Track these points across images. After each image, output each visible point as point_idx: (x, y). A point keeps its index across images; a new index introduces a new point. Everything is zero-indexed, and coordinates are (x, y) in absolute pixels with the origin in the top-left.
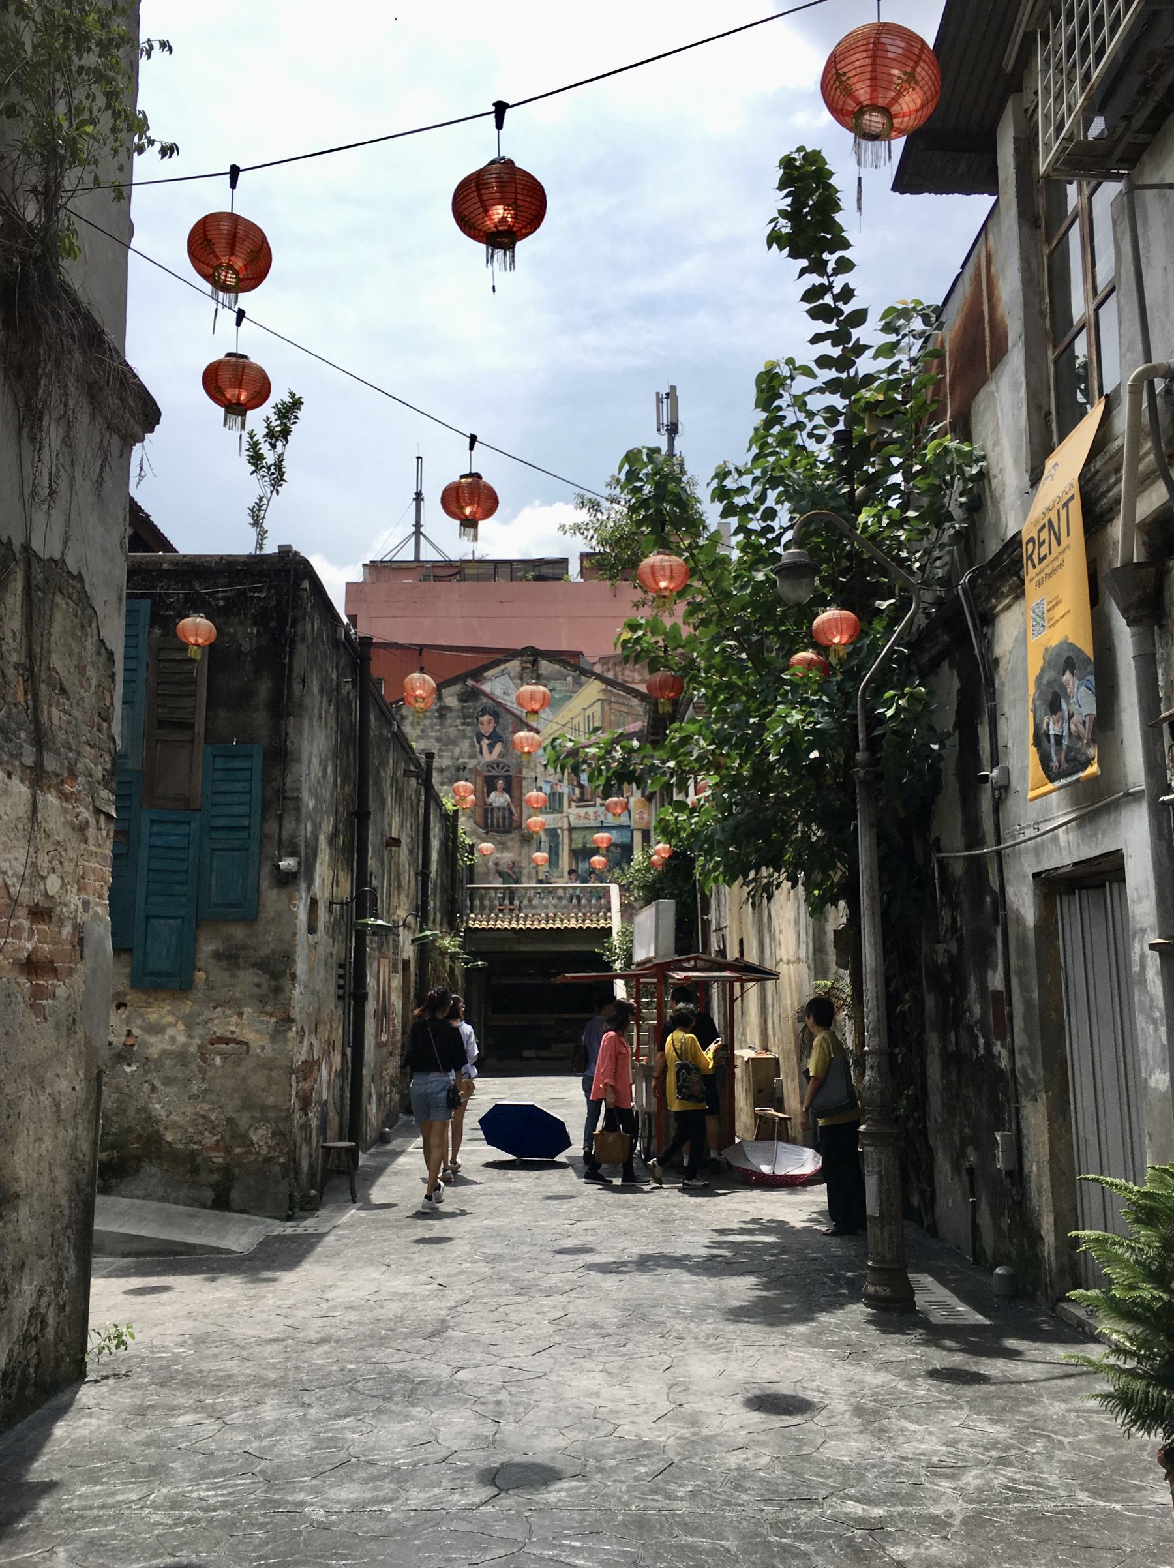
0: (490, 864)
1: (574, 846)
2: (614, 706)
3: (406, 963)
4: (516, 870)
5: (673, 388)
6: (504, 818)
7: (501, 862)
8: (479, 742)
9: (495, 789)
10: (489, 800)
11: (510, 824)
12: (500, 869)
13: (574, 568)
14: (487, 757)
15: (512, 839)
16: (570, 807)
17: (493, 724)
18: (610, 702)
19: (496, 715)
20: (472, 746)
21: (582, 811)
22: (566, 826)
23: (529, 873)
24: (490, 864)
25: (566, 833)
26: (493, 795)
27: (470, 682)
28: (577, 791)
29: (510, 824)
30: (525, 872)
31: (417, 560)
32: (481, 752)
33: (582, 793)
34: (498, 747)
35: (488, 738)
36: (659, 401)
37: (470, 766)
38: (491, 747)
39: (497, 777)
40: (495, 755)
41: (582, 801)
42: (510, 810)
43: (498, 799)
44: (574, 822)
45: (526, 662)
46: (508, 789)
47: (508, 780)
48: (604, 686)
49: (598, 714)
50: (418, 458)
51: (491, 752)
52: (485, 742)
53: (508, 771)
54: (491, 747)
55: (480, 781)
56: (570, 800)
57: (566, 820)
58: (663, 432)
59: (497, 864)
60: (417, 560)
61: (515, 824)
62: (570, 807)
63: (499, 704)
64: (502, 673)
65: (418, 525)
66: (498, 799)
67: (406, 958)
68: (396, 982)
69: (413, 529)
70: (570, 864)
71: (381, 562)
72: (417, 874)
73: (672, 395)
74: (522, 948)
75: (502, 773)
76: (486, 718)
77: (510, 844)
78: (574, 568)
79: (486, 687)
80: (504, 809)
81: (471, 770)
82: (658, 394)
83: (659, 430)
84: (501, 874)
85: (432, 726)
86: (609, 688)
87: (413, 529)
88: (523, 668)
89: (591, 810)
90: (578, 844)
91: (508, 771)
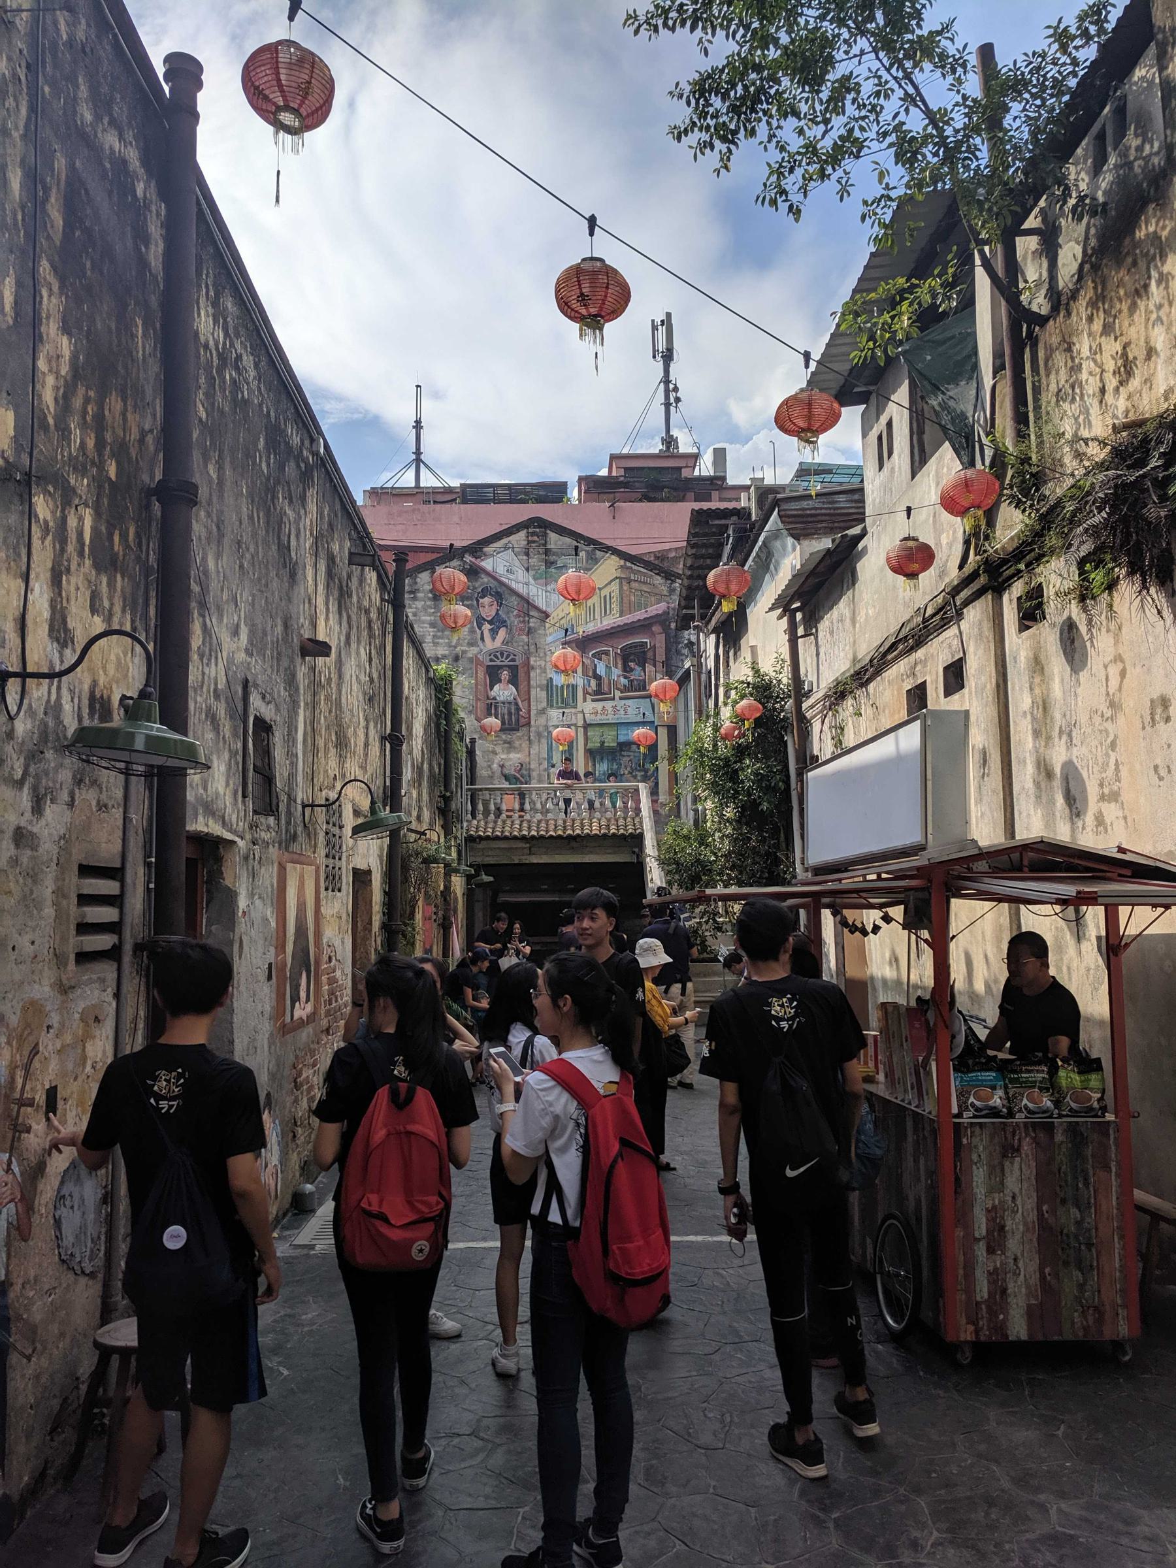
0: (495, 766)
1: (590, 745)
2: (634, 585)
3: (361, 877)
4: (524, 772)
5: (669, 315)
6: (510, 714)
7: (507, 764)
8: (480, 628)
9: (500, 681)
10: (492, 694)
11: (518, 720)
12: (506, 771)
13: (574, 493)
14: (490, 645)
15: (520, 738)
16: (585, 700)
17: (495, 606)
18: (629, 581)
19: (499, 597)
20: (472, 631)
21: (599, 706)
22: (581, 723)
23: (539, 775)
24: (495, 766)
25: (581, 730)
26: (496, 687)
27: (468, 558)
28: (593, 682)
29: (518, 720)
30: (534, 774)
31: (418, 486)
32: (482, 639)
33: (599, 685)
34: (502, 633)
35: (490, 622)
36: (654, 328)
37: (470, 655)
38: (494, 633)
39: (500, 667)
40: (498, 643)
41: (599, 693)
42: (517, 704)
43: (503, 692)
44: (590, 719)
45: (533, 534)
46: (514, 681)
47: (514, 670)
48: (622, 562)
49: (615, 594)
50: (418, 386)
51: (494, 639)
52: (487, 627)
53: (513, 660)
54: (494, 633)
55: (481, 673)
56: (585, 693)
57: (580, 716)
58: (659, 358)
59: (502, 766)
60: (418, 486)
61: (522, 721)
62: (585, 700)
63: (502, 584)
64: (506, 548)
65: (418, 452)
66: (503, 692)
67: (362, 865)
68: (338, 905)
69: (414, 457)
70: (586, 765)
71: (382, 488)
72: (383, 739)
73: (667, 322)
74: (535, 860)
75: (506, 663)
76: (486, 600)
77: (517, 744)
78: (574, 493)
79: (487, 564)
80: (510, 703)
81: (471, 660)
82: (653, 321)
83: (654, 357)
84: (507, 778)
85: (425, 608)
86: (628, 564)
87: (414, 457)
88: (529, 542)
89: (609, 705)
90: (594, 744)
91: (513, 660)
